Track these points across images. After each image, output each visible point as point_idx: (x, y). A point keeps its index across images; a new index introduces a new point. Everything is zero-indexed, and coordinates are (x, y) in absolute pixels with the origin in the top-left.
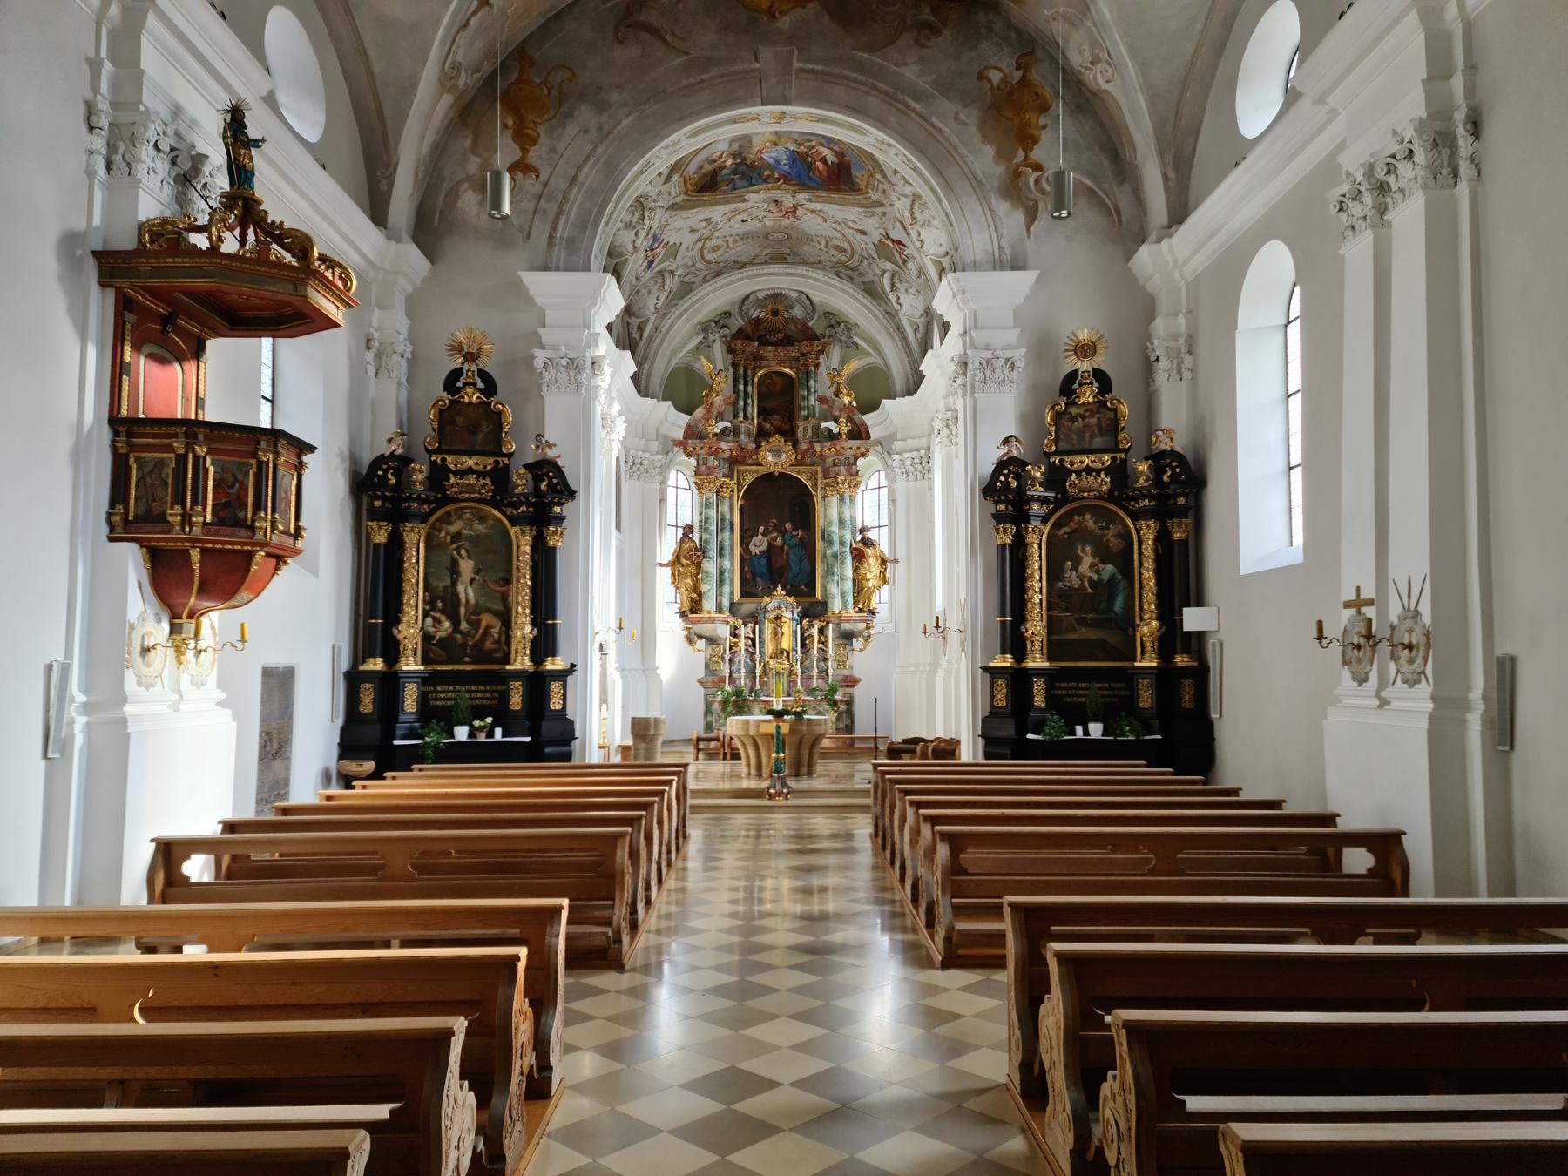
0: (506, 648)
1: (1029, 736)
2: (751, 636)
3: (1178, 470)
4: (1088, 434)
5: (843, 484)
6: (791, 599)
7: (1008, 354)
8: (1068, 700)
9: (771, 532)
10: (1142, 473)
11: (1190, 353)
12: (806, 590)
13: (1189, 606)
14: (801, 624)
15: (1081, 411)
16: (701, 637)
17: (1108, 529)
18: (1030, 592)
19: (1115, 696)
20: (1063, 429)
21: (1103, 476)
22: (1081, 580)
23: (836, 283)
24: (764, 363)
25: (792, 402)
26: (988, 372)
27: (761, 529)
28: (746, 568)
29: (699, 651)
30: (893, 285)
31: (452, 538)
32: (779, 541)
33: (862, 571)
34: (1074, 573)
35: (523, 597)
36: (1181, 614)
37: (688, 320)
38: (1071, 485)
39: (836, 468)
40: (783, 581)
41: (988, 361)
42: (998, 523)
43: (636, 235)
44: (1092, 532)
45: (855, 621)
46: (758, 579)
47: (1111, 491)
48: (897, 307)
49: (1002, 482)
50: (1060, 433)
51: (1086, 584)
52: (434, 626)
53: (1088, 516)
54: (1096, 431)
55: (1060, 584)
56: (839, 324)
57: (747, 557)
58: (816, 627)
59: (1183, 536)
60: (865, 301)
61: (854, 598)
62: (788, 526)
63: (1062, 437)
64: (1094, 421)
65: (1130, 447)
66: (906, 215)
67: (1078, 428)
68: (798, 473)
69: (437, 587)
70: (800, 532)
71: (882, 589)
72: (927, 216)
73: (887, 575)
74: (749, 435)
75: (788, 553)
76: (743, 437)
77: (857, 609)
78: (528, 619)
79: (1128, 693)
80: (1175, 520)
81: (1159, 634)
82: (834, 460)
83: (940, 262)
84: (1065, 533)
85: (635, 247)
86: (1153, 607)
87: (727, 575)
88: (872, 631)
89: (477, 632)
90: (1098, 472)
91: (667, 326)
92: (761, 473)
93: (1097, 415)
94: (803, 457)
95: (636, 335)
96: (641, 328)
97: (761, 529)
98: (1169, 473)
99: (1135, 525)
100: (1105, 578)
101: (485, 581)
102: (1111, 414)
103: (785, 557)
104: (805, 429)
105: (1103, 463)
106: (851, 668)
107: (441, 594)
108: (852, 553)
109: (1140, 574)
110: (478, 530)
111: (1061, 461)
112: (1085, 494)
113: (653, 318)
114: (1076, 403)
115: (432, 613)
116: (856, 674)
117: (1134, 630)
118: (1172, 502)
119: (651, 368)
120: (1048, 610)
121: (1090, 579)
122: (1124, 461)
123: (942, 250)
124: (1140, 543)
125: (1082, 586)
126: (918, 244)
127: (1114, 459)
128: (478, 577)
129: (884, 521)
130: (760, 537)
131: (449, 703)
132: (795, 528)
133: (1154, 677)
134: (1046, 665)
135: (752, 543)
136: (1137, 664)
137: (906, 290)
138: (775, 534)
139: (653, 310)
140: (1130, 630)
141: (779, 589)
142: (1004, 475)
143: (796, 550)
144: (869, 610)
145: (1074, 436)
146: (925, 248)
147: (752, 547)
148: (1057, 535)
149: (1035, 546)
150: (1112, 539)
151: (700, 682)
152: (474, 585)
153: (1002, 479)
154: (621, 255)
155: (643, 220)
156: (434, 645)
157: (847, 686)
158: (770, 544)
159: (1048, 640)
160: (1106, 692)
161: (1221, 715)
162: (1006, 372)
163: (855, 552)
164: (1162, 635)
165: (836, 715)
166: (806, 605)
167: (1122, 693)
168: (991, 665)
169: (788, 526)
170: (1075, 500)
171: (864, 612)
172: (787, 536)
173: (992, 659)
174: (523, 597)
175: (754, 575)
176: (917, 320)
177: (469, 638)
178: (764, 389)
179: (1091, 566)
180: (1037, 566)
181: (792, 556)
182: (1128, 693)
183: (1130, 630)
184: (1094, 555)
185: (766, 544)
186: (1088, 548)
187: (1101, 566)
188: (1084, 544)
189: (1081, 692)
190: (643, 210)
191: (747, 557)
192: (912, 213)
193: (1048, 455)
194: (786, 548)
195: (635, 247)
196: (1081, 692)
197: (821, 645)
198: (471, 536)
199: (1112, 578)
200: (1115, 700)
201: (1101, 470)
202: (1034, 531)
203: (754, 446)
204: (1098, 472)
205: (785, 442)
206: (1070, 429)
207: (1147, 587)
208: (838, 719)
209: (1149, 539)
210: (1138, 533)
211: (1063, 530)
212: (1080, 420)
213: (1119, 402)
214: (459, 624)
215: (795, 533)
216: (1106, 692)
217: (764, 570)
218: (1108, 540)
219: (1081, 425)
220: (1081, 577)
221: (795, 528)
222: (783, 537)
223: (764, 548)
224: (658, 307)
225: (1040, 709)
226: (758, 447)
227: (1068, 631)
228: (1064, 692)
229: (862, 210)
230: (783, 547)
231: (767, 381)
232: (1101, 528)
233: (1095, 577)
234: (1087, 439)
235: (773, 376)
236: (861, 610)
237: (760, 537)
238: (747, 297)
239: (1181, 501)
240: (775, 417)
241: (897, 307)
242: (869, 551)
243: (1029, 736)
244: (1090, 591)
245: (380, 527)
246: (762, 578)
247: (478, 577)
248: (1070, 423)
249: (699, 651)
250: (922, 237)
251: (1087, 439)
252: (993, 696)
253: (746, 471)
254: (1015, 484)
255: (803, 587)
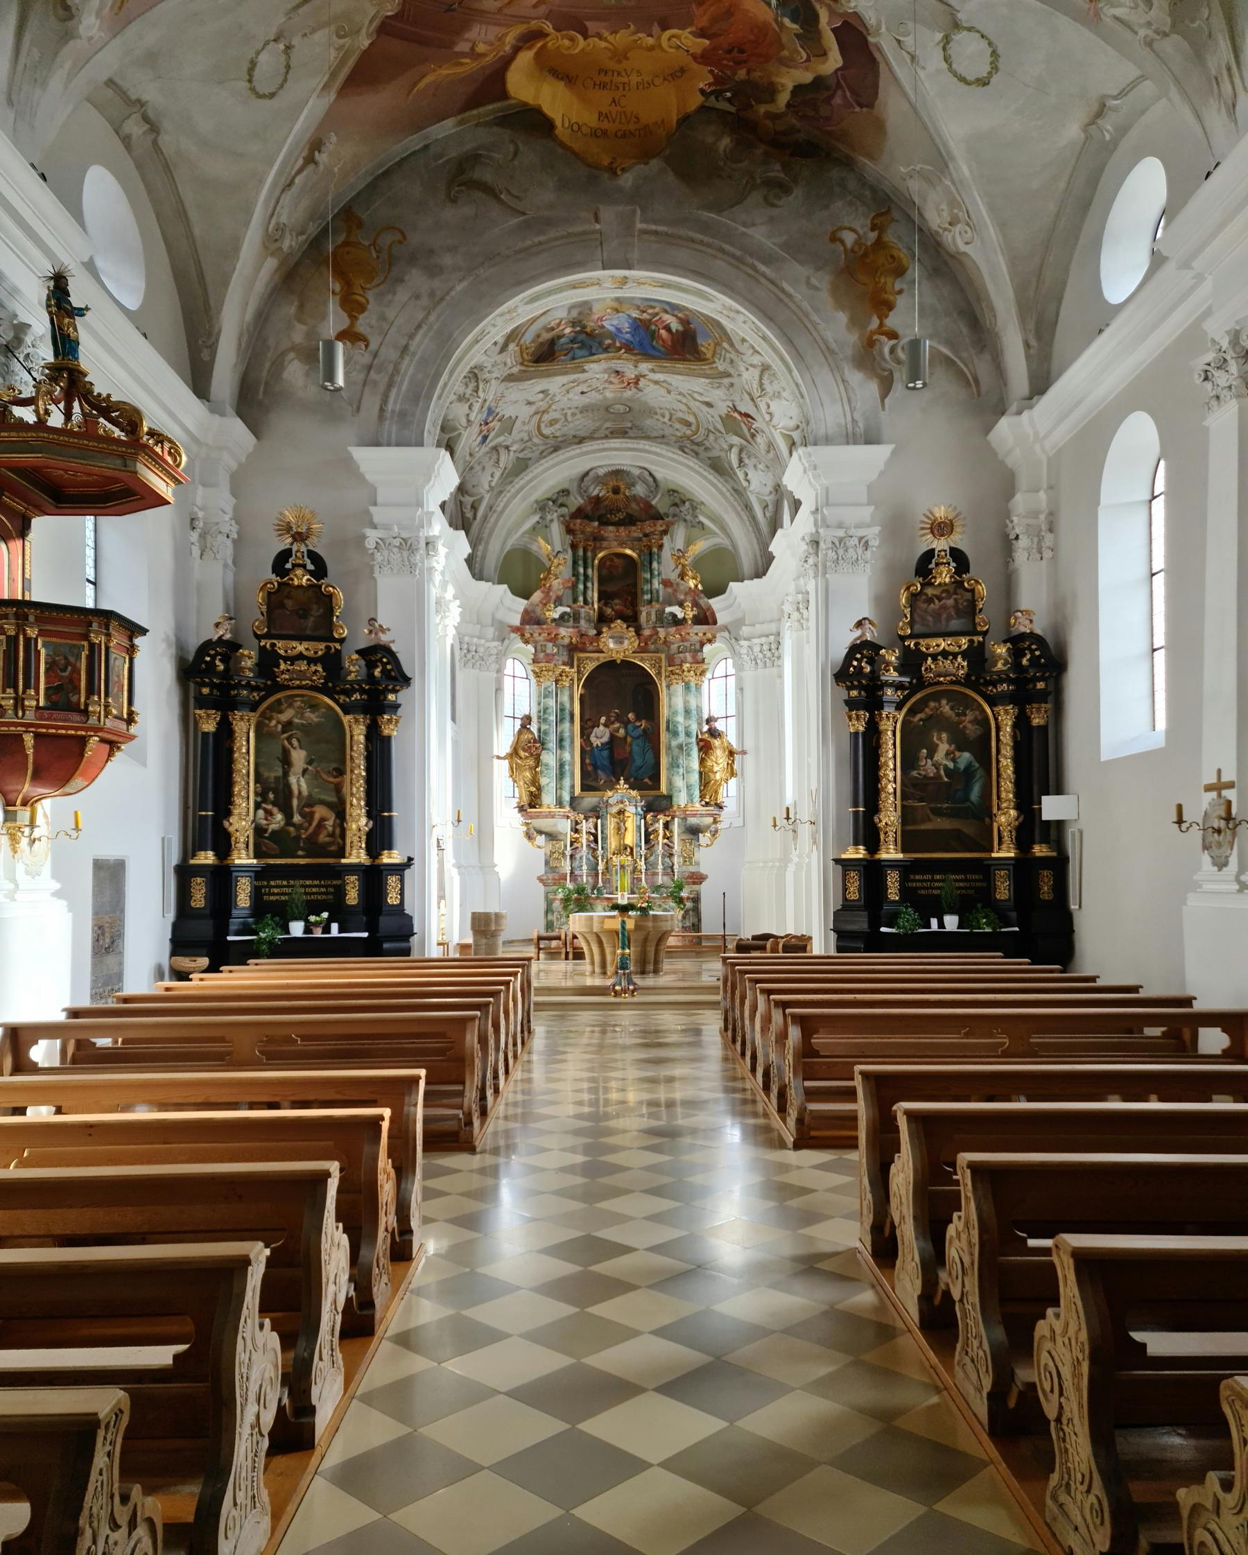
0: (340, 841)
1: (883, 929)
2: (593, 831)
3: (1037, 653)
4: (944, 616)
5: (689, 671)
6: (634, 793)
7: (861, 533)
8: (923, 892)
9: (613, 723)
10: (1000, 656)
11: (1051, 530)
12: (650, 783)
13: (1048, 794)
14: (645, 818)
15: (937, 592)
16: (540, 832)
17: (965, 715)
18: (884, 782)
19: (970, 888)
20: (918, 611)
21: (959, 659)
22: (937, 768)
23: (681, 459)
24: (605, 544)
25: (635, 585)
26: (841, 552)
27: (603, 720)
28: (588, 761)
29: (539, 847)
30: (741, 461)
31: (283, 726)
32: (622, 732)
33: (709, 763)
34: (929, 761)
35: (358, 789)
36: (1040, 803)
37: (524, 499)
38: (926, 669)
39: (681, 655)
40: (626, 773)
41: (841, 540)
42: (851, 710)
43: (470, 407)
44: (947, 719)
45: (702, 815)
46: (600, 772)
47: (968, 675)
48: (745, 484)
49: (854, 667)
50: (915, 615)
51: (942, 773)
52: (266, 819)
53: (944, 702)
54: (953, 613)
55: (914, 773)
56: (684, 502)
57: (588, 749)
58: (661, 821)
59: (1042, 722)
60: (711, 477)
61: (701, 791)
62: (631, 716)
63: (917, 619)
64: (950, 602)
65: (987, 630)
66: (755, 386)
67: (933, 610)
68: (641, 661)
69: (268, 778)
70: (643, 722)
71: (729, 782)
72: (776, 387)
73: (735, 767)
74: (589, 621)
75: (631, 745)
76: (583, 622)
77: (703, 803)
78: (363, 811)
79: (984, 884)
80: (1035, 705)
81: (1017, 823)
82: (679, 647)
83: (790, 436)
84: (921, 720)
85: (469, 421)
86: (1011, 796)
87: (567, 767)
88: (719, 826)
89: (310, 824)
90: (955, 655)
91: (502, 504)
92: (602, 661)
93: (954, 596)
94: (646, 644)
95: (469, 515)
96: (474, 508)
97: (603, 720)
98: (1028, 656)
99: (993, 711)
100: (962, 766)
101: (318, 772)
102: (968, 595)
103: (628, 748)
104: (649, 614)
105: (960, 647)
106: (698, 864)
107: (273, 785)
108: (698, 744)
109: (998, 762)
110: (309, 718)
111: (917, 644)
112: (942, 679)
113: (487, 497)
114: (932, 584)
115: (264, 805)
116: (703, 870)
117: (991, 819)
118: (1031, 686)
119: (486, 549)
120: (902, 799)
121: (946, 767)
122: (982, 645)
123: (792, 424)
124: (998, 729)
125: (938, 776)
126: (767, 417)
127: (971, 642)
128: (310, 768)
129: (732, 710)
130: (601, 728)
131: (283, 898)
132: (638, 718)
133: (1011, 867)
134: (900, 856)
135: (593, 734)
136: (994, 855)
137: (755, 466)
138: (617, 725)
139: (487, 487)
140: (987, 820)
141: (622, 782)
142: (857, 660)
143: (640, 741)
144: (716, 804)
145: (930, 619)
146: (775, 421)
147: (593, 739)
148: (912, 722)
149: (889, 733)
150: (969, 726)
151: (540, 879)
152: (306, 776)
153: (855, 663)
154: (455, 429)
155: (477, 391)
156: (266, 838)
157: (694, 883)
158: (612, 737)
159: (903, 831)
160: (961, 884)
161: (1080, 907)
162: (860, 551)
163: (702, 744)
164: (1020, 824)
165: (682, 912)
166: (650, 798)
167: (979, 884)
168: (844, 856)
169: (631, 716)
170: (931, 685)
171: (711, 806)
172: (630, 727)
173: (845, 851)
174: (358, 789)
175: (595, 767)
176: (767, 498)
177: (303, 831)
178: (605, 572)
179: (947, 754)
180: (890, 754)
181: (635, 748)
182: (984, 884)
183: (987, 820)
184: (950, 743)
185: (608, 735)
186: (944, 735)
187: (957, 754)
188: (940, 731)
189: (936, 884)
190: (477, 381)
191: (588, 749)
192: (761, 385)
193: (903, 638)
194: (629, 739)
195: (469, 421)
196: (936, 884)
197: (666, 841)
198: (302, 724)
199: (969, 766)
200: (971, 892)
201: (958, 654)
202: (888, 717)
203: (595, 632)
204: (955, 655)
205: (627, 628)
206: (926, 611)
207: (1004, 775)
208: (684, 917)
209: (1006, 725)
210: (996, 719)
211: (919, 717)
212: (936, 601)
213: (977, 582)
214: (292, 818)
215: (638, 724)
216: (961, 884)
217: (606, 763)
218: (965, 727)
219: (937, 607)
220: (936, 765)
221: (638, 718)
222: (626, 728)
223: (606, 739)
224: (493, 484)
225: (894, 901)
226: (599, 633)
227: (923, 822)
228: (919, 884)
229: (708, 381)
230: (625, 738)
231: (608, 563)
232: (958, 715)
233: (951, 765)
234: (944, 622)
235: (616, 560)
236: (707, 804)
237: (601, 728)
238: (587, 474)
239: (1040, 685)
240: (617, 601)
241: (745, 484)
242: (717, 742)
243: (883, 929)
244: (946, 779)
245: (208, 716)
246: (603, 770)
247: (310, 768)
248: (926, 605)
249: (539, 847)
250: (749, 477)
251: (944, 622)
252: (845, 889)
253: (587, 658)
254: (868, 669)
255: (646, 780)
